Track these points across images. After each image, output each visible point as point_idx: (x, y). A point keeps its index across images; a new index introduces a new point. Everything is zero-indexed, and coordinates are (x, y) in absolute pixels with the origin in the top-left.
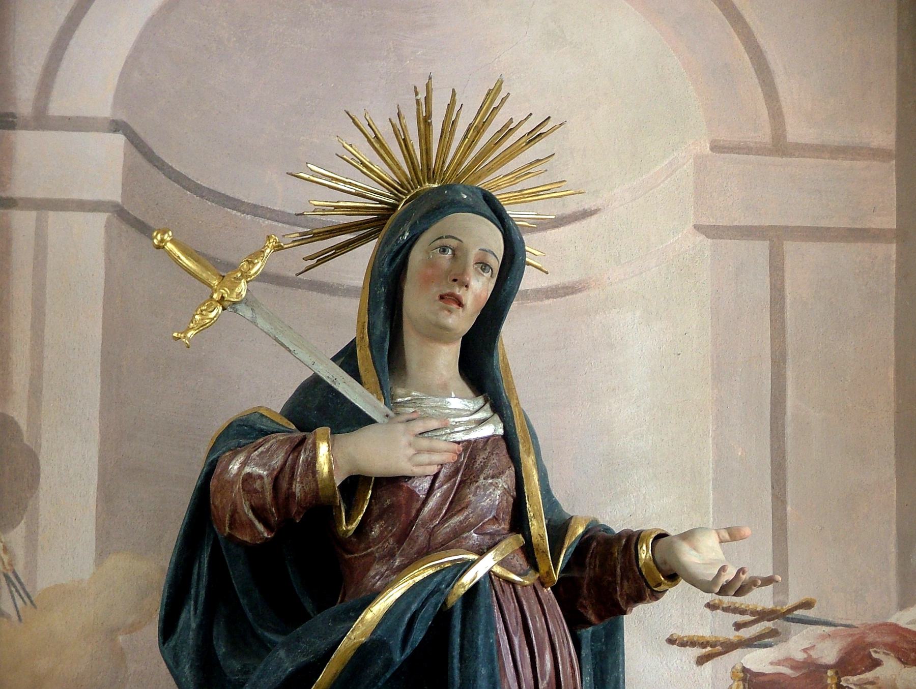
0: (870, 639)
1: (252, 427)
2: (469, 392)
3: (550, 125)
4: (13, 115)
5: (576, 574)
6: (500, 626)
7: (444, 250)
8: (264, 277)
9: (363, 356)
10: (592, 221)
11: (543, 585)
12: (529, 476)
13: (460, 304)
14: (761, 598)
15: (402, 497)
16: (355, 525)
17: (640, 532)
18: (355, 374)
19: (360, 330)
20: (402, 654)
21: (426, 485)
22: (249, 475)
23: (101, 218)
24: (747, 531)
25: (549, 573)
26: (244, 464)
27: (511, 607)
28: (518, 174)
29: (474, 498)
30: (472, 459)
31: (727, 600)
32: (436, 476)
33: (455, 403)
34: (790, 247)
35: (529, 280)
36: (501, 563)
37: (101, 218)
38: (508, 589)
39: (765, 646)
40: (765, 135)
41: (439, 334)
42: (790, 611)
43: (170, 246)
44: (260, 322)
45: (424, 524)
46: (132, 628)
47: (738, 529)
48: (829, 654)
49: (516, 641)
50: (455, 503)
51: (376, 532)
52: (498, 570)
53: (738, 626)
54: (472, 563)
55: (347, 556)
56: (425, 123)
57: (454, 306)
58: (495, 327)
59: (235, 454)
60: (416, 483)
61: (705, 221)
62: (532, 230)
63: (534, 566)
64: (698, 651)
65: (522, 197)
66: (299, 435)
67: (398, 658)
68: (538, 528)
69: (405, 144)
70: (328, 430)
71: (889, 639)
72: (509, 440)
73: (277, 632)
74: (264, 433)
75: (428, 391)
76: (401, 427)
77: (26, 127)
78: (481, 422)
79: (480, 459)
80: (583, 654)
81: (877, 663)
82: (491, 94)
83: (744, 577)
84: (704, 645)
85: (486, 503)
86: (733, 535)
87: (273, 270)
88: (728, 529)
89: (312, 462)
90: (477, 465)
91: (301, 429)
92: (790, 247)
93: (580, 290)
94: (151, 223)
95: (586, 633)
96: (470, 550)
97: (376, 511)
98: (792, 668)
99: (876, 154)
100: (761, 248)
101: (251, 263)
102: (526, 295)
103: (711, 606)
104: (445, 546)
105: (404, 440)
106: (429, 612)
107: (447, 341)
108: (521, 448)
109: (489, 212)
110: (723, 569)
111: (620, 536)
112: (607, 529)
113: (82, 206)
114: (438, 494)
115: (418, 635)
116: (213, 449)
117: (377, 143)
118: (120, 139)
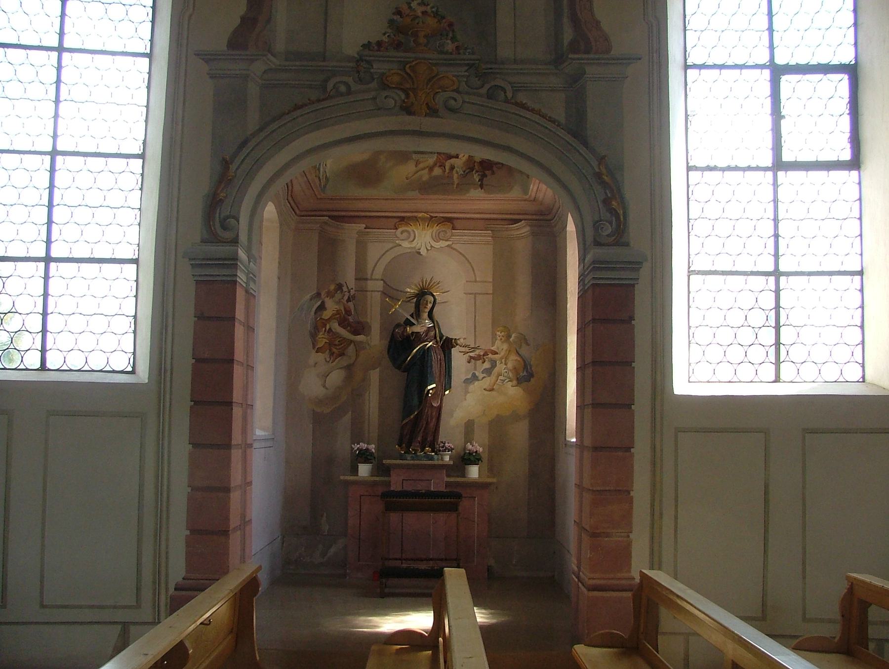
18: (413, 318)
28: (437, 288)
33: (427, 321)
34: (477, 296)
36: (433, 343)
68: (438, 339)
69: (426, 283)
78: (430, 324)
81: (488, 355)
84: (464, 352)
89: (407, 330)
93: (587, 148)
100: (473, 296)
102: (438, 303)
118: (382, 282)
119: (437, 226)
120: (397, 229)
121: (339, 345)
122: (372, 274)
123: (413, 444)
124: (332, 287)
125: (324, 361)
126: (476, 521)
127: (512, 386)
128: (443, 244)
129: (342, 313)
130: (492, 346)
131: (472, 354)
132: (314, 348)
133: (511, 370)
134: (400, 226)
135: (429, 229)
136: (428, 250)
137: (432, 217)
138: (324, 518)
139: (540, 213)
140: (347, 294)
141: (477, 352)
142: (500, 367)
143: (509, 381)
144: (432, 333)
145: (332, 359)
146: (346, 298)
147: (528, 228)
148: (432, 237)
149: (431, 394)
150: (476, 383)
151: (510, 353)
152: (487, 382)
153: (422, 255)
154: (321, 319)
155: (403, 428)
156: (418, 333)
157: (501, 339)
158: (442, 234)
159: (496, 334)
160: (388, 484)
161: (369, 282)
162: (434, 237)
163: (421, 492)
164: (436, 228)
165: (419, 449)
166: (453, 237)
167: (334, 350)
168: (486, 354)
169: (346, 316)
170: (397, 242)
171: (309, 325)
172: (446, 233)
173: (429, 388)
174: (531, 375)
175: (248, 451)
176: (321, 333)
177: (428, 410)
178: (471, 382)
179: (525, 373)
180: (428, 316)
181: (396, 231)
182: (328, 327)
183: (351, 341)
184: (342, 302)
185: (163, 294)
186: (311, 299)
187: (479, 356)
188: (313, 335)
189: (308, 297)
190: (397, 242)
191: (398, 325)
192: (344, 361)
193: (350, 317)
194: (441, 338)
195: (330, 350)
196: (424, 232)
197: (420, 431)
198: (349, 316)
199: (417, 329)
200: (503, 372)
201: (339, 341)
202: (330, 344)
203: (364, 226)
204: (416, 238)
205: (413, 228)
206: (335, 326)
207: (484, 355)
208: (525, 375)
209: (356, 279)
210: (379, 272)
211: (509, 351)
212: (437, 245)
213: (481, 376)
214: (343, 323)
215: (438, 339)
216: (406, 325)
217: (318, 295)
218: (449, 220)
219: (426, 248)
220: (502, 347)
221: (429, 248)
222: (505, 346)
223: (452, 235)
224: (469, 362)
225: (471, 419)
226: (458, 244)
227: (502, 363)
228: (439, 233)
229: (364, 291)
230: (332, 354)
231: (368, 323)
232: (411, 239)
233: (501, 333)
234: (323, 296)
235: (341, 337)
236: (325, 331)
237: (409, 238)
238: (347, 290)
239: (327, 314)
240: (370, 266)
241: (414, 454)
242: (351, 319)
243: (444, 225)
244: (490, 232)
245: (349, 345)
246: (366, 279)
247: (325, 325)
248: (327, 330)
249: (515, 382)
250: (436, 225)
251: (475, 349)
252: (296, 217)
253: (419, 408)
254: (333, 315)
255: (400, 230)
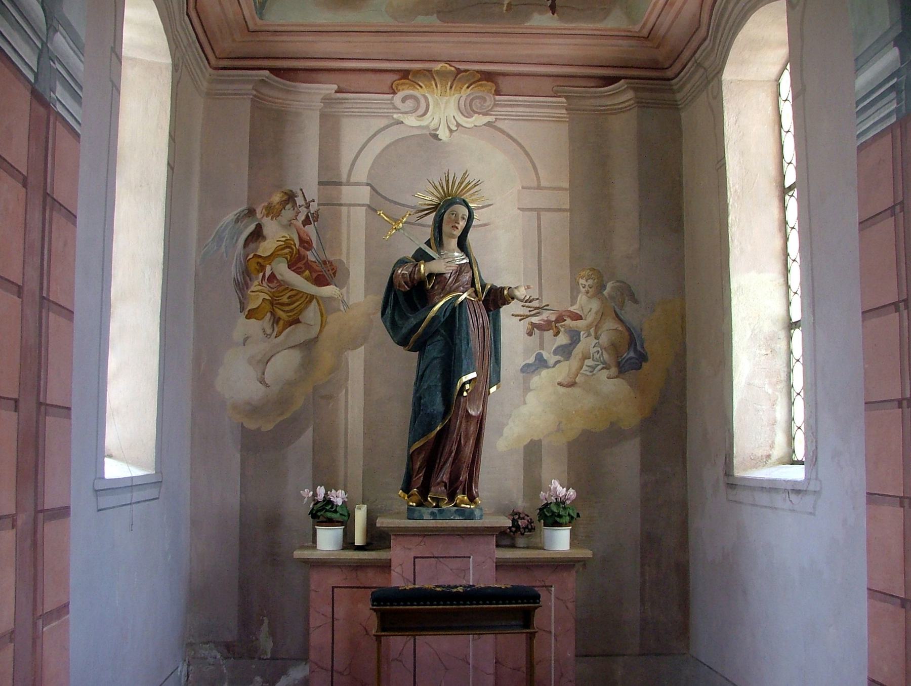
0: (563, 314)
1: (404, 261)
2: (460, 251)
3: (480, 182)
4: (341, 182)
5: (488, 298)
6: (469, 311)
7: (453, 214)
8: (405, 222)
9: (432, 242)
10: (491, 206)
11: (480, 301)
12: (476, 272)
13: (457, 228)
14: (535, 304)
15: (443, 278)
16: (431, 286)
17: (504, 287)
18: (430, 247)
19: (431, 235)
20: (444, 318)
21: (449, 275)
22: (403, 273)
23: (364, 208)
24: (532, 286)
25: (481, 298)
26: (402, 271)
27: (471, 307)
28: (473, 194)
29: (460, 223)
30: (461, 268)
31: (527, 304)
32: (451, 273)
33: (456, 254)
34: (542, 213)
35: (475, 223)
36: (469, 295)
37: (364, 208)
38: (471, 302)
39: (537, 316)
40: (535, 184)
41: (452, 236)
42: (543, 307)
43: (382, 214)
44: (406, 234)
45: (449, 285)
46: (374, 314)
47: (529, 286)
48: (553, 318)
49: (473, 315)
50: (457, 280)
51: (436, 288)
52: (468, 297)
53: (530, 311)
54: (461, 295)
55: (428, 294)
56: (447, 181)
57: (455, 229)
58: (595, 281)
59: (400, 268)
60: (446, 275)
61: (520, 207)
62: (476, 209)
63: (477, 296)
64: (520, 318)
65: (473, 202)
66: (416, 263)
67: (442, 320)
68: (478, 286)
69: (442, 188)
70: (423, 261)
71: (568, 314)
72: (470, 263)
73: (411, 314)
74: (407, 262)
75: (449, 251)
76: (442, 260)
77: (344, 185)
78: (463, 259)
79: (463, 268)
80: (490, 318)
81: (565, 320)
82: (464, 174)
83: (531, 298)
85: (464, 280)
86: (528, 287)
87: (409, 221)
88: (527, 286)
90: (462, 270)
91: (416, 261)
92: (542, 213)
93: (487, 225)
94: (377, 209)
95: (491, 313)
96: (460, 292)
97: (436, 282)
98: (544, 322)
99: (566, 189)
100: (535, 213)
101: (403, 219)
102: (474, 226)
103: (523, 306)
104: (454, 291)
105: (443, 264)
106: (450, 308)
107: (454, 238)
108: (474, 266)
109: (464, 204)
110: (526, 296)
111: (499, 288)
112: (496, 286)
113: (359, 205)
114: (452, 278)
115: (448, 314)
116: (394, 267)
117: (436, 188)
118: (369, 188)
119: (468, 87)
120: (394, 93)
121: (288, 304)
122: (349, 175)
123: (433, 489)
124: (277, 198)
125: (261, 332)
126: (553, 631)
127: (608, 378)
128: (482, 120)
129: (295, 245)
130: (571, 306)
131: (535, 320)
132: (242, 309)
133: (605, 348)
134: (400, 87)
135: (454, 95)
136: (451, 131)
137: (459, 71)
138: (265, 627)
139: (655, 66)
140: (304, 211)
141: (545, 315)
142: (587, 343)
143: (603, 368)
144: (466, 277)
145: (276, 330)
146: (302, 217)
147: (630, 95)
148: (459, 109)
149: (467, 391)
150: (544, 372)
151: (603, 318)
152: (563, 371)
153: (440, 140)
154: (255, 256)
155: (411, 458)
156: (441, 275)
157: (587, 292)
158: (477, 102)
159: (578, 283)
160: (385, 567)
161: (345, 189)
162: (462, 106)
163: (455, 590)
164: (465, 92)
165: (447, 499)
166: (499, 109)
167: (280, 313)
168: (560, 319)
169: (302, 250)
170: (395, 116)
171: (233, 269)
172: (485, 101)
173: (465, 379)
174: (642, 357)
175: (50, 529)
176: (256, 283)
177: (461, 423)
178: (534, 371)
179: (632, 354)
180: (458, 246)
181: (393, 97)
182: (268, 273)
183: (311, 298)
184: (295, 226)
185: (452, 535)
186: (237, 221)
187: (549, 322)
188: (242, 286)
189: (231, 216)
190: (395, 116)
191: (402, 262)
192: (299, 334)
193: (308, 253)
194: (483, 287)
195: (273, 314)
196: (445, 99)
197: (445, 463)
198: (308, 250)
199: (437, 266)
200: (591, 352)
201: (289, 297)
202: (272, 303)
203: (335, 87)
204: (431, 107)
205: (424, 91)
206: (282, 269)
207: (557, 321)
208: (631, 358)
209: (320, 183)
210: (361, 173)
211: (602, 315)
212: (468, 122)
213: (551, 359)
214: (297, 263)
215: (478, 286)
216: (418, 260)
217: (251, 212)
218: (489, 76)
219: (448, 127)
220: (590, 307)
221: (454, 128)
222: (595, 305)
223: (495, 105)
224: (530, 334)
225: (536, 439)
226: (506, 121)
227: (589, 335)
228: (472, 100)
229: (333, 204)
230: (276, 320)
231: (341, 262)
232: (421, 111)
233: (587, 281)
234: (259, 215)
235: (292, 290)
236: (264, 276)
237: (416, 110)
238: (303, 203)
239: (266, 248)
240: (347, 157)
241: (435, 507)
242: (311, 256)
243: (481, 85)
244: (563, 100)
245: (310, 301)
246: (340, 184)
247: (262, 268)
248: (267, 276)
249: (614, 370)
250: (467, 85)
251: (540, 309)
252: (210, 70)
253: (444, 418)
254: (279, 249)
255: (400, 95)
